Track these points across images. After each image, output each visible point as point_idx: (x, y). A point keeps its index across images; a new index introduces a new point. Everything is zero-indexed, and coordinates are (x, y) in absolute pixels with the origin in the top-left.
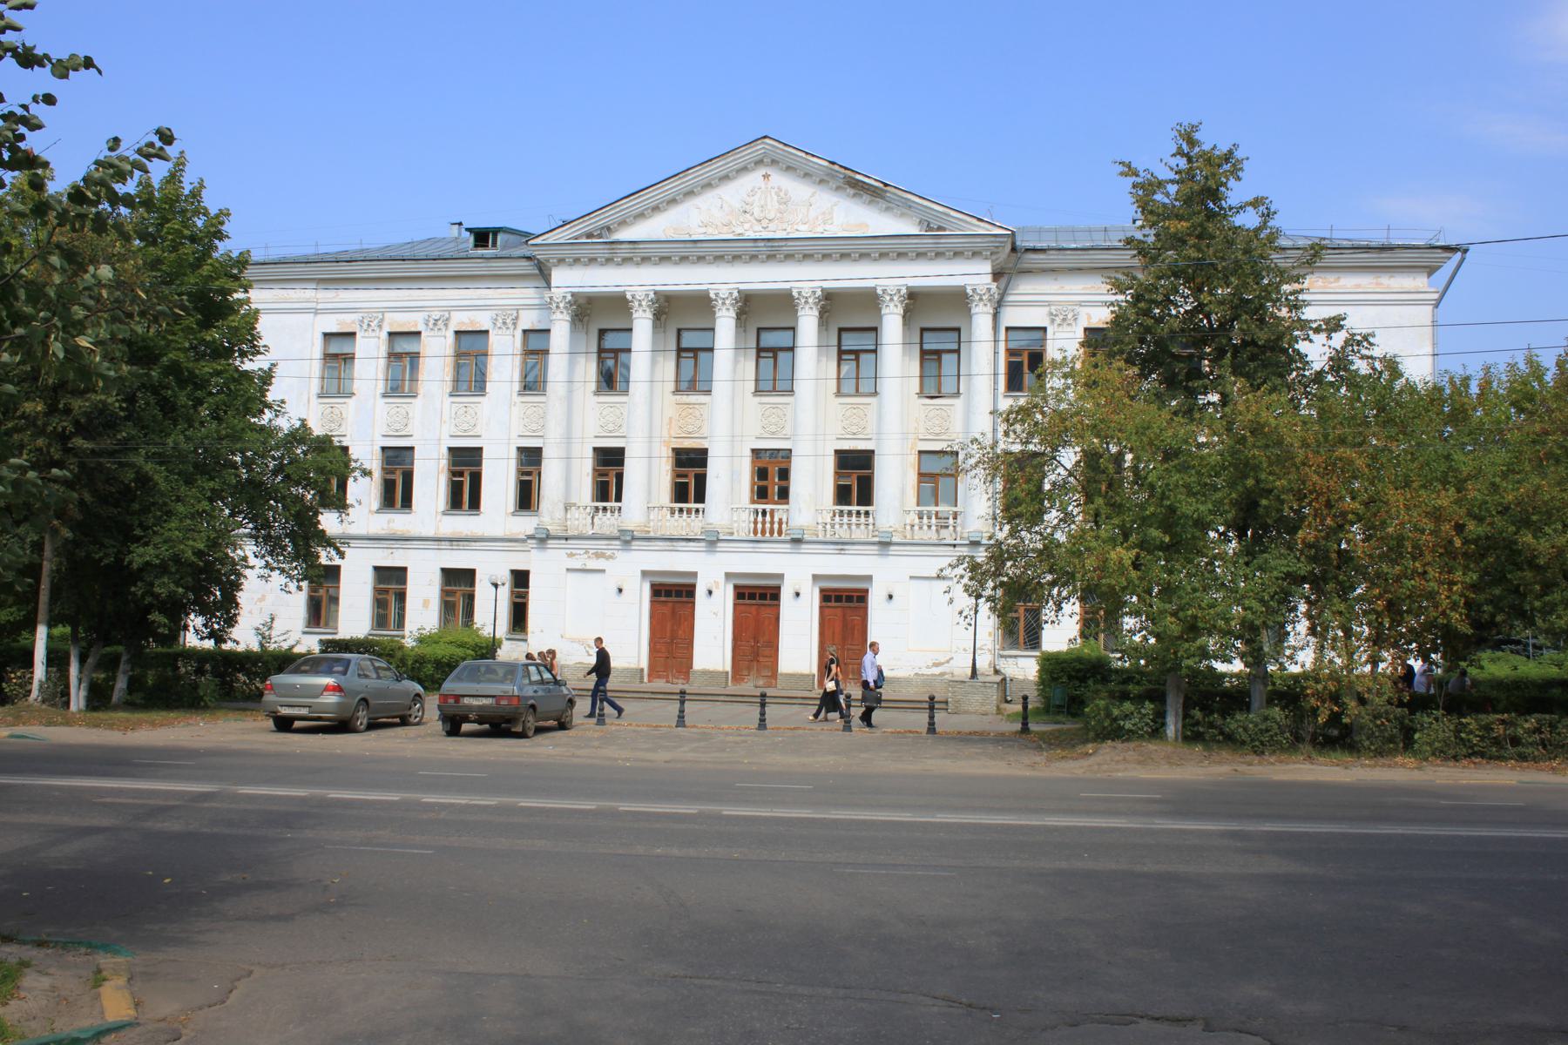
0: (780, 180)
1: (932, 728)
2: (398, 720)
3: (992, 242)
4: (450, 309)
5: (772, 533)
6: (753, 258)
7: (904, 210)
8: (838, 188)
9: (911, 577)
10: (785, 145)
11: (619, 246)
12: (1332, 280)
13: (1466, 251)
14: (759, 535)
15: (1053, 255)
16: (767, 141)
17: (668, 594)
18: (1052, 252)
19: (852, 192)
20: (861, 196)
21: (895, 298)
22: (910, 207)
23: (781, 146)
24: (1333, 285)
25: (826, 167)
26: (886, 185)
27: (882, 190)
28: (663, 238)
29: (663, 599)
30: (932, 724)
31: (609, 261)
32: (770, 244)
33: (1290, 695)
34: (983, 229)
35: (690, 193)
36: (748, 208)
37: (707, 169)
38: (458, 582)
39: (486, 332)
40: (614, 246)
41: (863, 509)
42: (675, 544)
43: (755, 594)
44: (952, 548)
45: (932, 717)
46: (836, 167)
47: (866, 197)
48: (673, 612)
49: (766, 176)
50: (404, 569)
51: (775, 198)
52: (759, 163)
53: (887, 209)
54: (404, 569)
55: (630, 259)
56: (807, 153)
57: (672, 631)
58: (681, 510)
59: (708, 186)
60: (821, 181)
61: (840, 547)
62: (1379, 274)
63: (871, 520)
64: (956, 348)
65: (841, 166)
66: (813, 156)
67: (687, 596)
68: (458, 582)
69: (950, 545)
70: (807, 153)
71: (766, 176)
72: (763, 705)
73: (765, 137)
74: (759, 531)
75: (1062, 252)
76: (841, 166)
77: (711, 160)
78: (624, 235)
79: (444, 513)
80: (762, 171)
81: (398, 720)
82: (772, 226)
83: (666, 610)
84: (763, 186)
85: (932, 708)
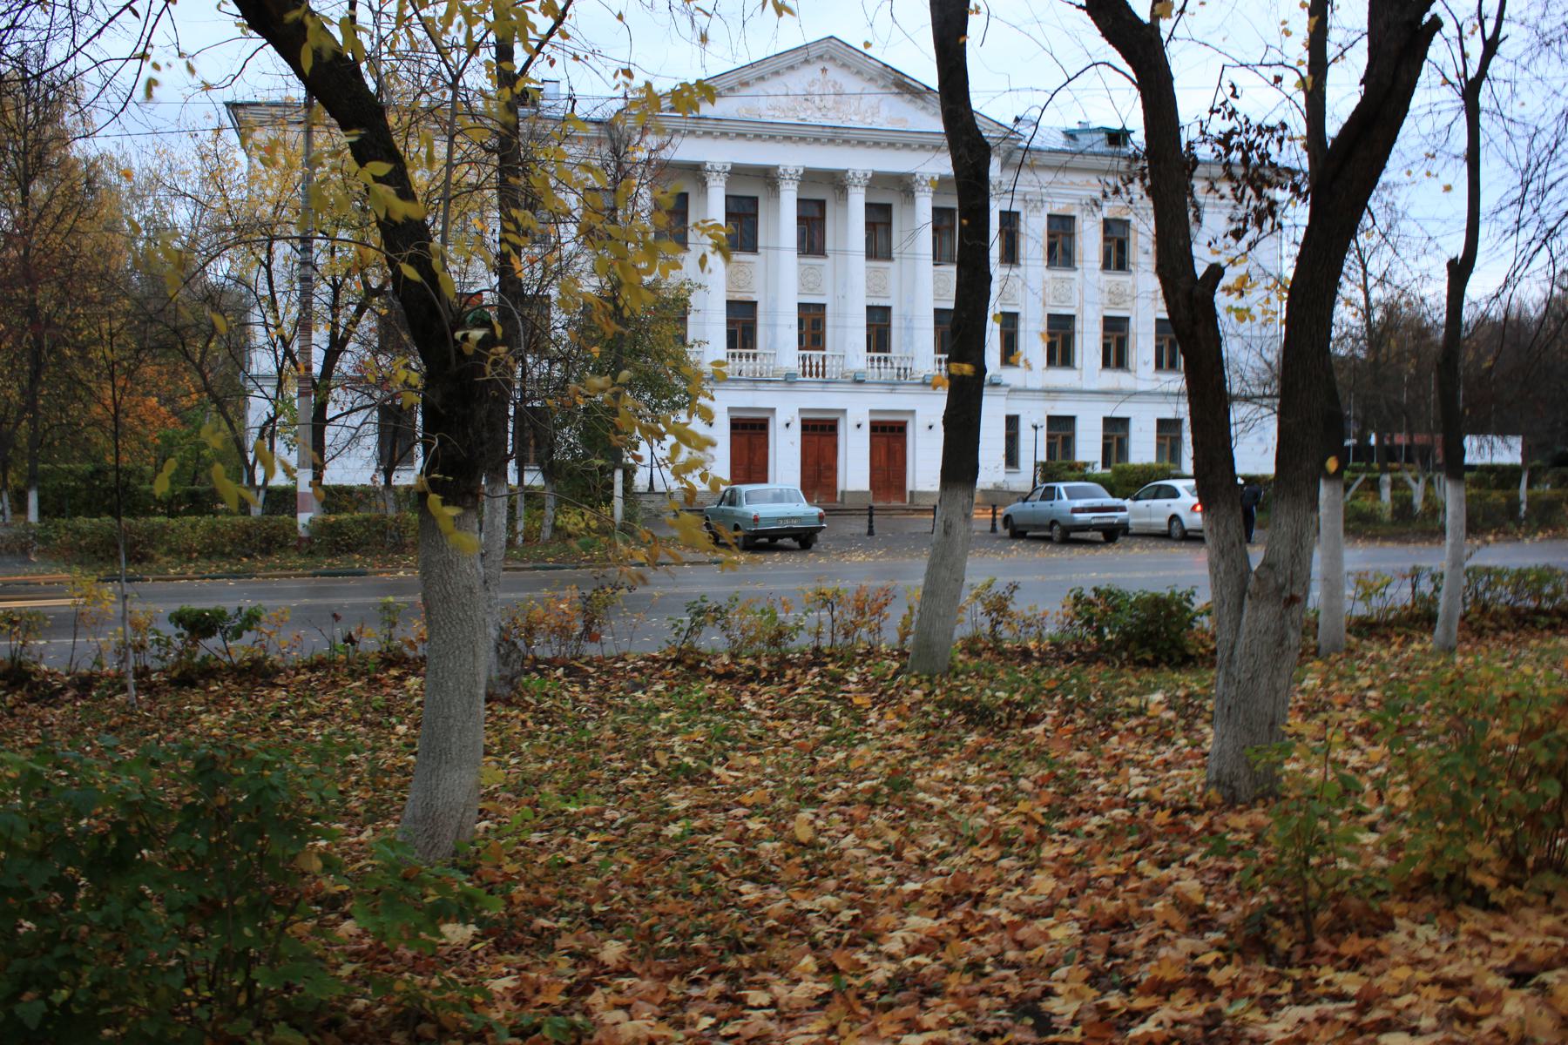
0: (835, 74)
2: (1073, 535)
6: (817, 140)
8: (884, 87)
28: (736, 116)
41: (882, 355)
47: (908, 97)
49: (824, 70)
52: (820, 57)
53: (923, 108)
58: (748, 356)
60: (871, 79)
68: (1116, 430)
71: (824, 70)
72: (871, 515)
80: (820, 65)
82: (831, 114)
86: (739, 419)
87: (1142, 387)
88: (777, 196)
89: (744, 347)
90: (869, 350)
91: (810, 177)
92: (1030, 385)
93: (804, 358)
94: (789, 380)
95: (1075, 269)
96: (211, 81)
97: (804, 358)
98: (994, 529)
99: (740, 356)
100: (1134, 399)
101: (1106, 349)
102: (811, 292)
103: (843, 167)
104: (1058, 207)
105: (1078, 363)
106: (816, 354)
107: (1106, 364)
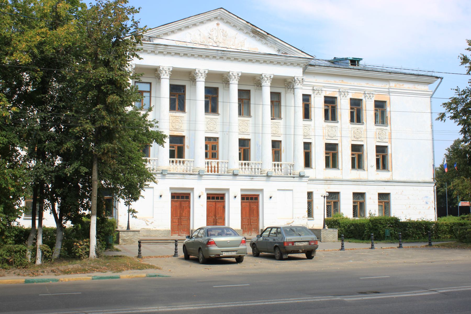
0: (223, 26)
3: (306, 61)
5: (215, 172)
7: (273, 45)
8: (247, 33)
9: (278, 190)
10: (229, 12)
11: (159, 46)
12: (401, 85)
13: (442, 78)
14: (213, 172)
15: (317, 68)
16: (222, 10)
17: (178, 197)
18: (317, 66)
19: (252, 35)
20: (255, 37)
21: (203, 75)
22: (276, 44)
23: (227, 13)
24: (402, 87)
25: (245, 24)
26: (268, 34)
27: (266, 36)
29: (176, 200)
31: (153, 52)
32: (223, 52)
34: (303, 55)
35: (187, 27)
36: (211, 37)
37: (197, 18)
40: (157, 46)
41: (246, 162)
42: (185, 176)
43: (214, 197)
44: (293, 178)
46: (249, 24)
47: (258, 38)
48: (181, 205)
49: (218, 24)
50: (229, 189)
51: (222, 34)
52: (216, 18)
54: (229, 189)
55: (162, 52)
56: (238, 17)
57: (180, 213)
59: (195, 25)
60: (240, 29)
61: (251, 178)
62: (415, 84)
63: (250, 167)
65: (251, 24)
66: (240, 18)
67: (186, 198)
69: (292, 177)
70: (238, 17)
73: (221, 8)
74: (216, 171)
75: (320, 67)
76: (251, 24)
77: (199, 15)
78: (156, 41)
80: (216, 22)
81: (234, 260)
83: (177, 204)
84: (217, 28)
86: (175, 194)
87: (371, 178)
88: (261, 89)
89: (178, 157)
90: (240, 160)
91: (244, 78)
92: (318, 177)
93: (208, 163)
94: (200, 175)
95: (338, 122)
96: (443, 80)
97: (208, 163)
98: (176, 255)
99: (176, 162)
100: (314, 182)
101: (327, 159)
102: (211, 131)
103: (227, 70)
104: (329, 93)
105: (340, 166)
106: (214, 162)
107: (327, 165)
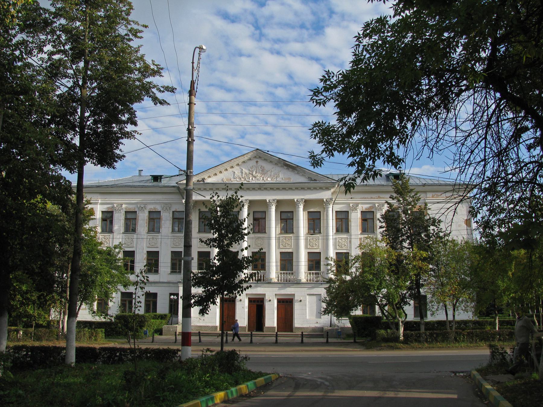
1: (327, 342)
4: (146, 204)
16: (258, 151)
19: (286, 168)
30: (251, 340)
33: (430, 326)
38: (151, 298)
39: (160, 212)
45: (251, 338)
47: (290, 169)
60: (276, 164)
64: (372, 217)
71: (257, 162)
79: (170, 274)
85: (200, 336)
